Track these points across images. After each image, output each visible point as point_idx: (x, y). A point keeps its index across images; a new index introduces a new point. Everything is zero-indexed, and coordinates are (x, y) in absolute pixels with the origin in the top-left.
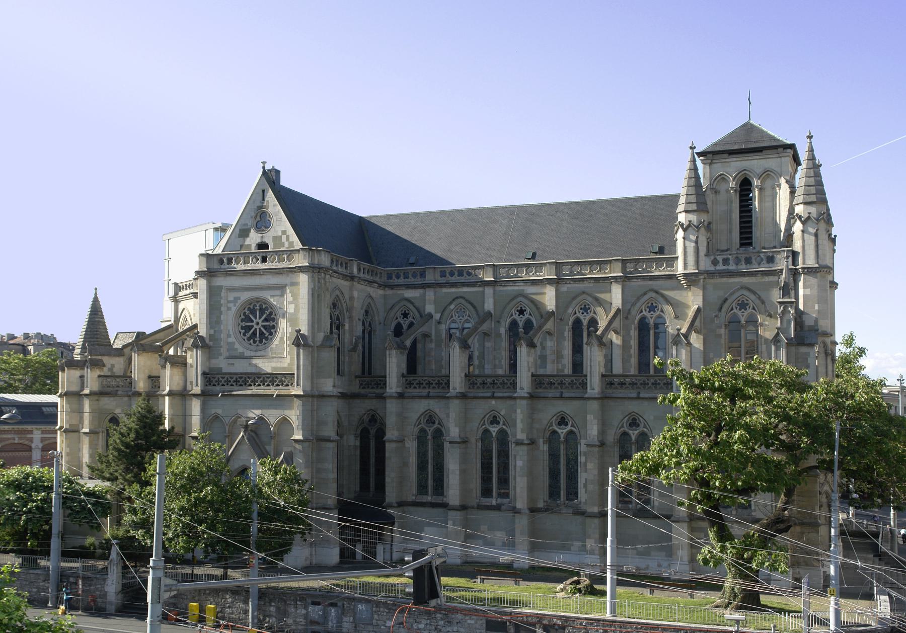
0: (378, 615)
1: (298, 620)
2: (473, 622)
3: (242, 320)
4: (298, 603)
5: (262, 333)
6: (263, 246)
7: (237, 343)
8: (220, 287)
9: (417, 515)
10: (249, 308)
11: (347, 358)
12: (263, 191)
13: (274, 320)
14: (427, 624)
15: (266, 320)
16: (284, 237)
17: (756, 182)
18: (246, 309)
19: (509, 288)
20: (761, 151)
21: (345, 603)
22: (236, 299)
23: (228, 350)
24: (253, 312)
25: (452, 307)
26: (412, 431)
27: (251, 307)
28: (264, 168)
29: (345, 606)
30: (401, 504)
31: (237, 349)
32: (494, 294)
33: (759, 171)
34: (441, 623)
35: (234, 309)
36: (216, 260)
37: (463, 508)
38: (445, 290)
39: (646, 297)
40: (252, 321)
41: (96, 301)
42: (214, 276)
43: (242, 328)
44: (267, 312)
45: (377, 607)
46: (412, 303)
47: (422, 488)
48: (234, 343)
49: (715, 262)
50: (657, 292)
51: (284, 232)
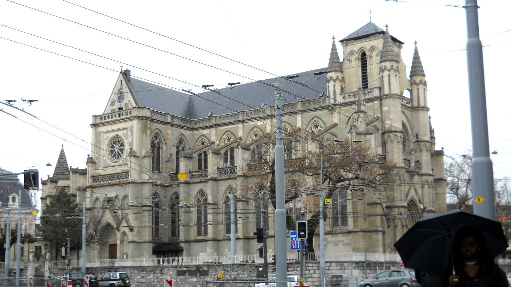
3: (111, 148)
6: (121, 109)
8: (101, 132)
9: (196, 246)
10: (113, 141)
11: (164, 166)
15: (120, 147)
16: (129, 103)
17: (368, 54)
19: (250, 123)
20: (368, 37)
22: (108, 137)
23: (104, 164)
24: (115, 143)
25: (224, 136)
26: (193, 201)
27: (114, 140)
28: (122, 69)
30: (187, 241)
32: (243, 127)
33: (369, 48)
34: (159, 274)
35: (107, 142)
36: (99, 118)
37: (214, 240)
38: (221, 128)
39: (313, 121)
41: (63, 151)
42: (98, 126)
45: (133, 269)
46: (206, 137)
47: (199, 233)
49: (344, 98)
50: (318, 117)
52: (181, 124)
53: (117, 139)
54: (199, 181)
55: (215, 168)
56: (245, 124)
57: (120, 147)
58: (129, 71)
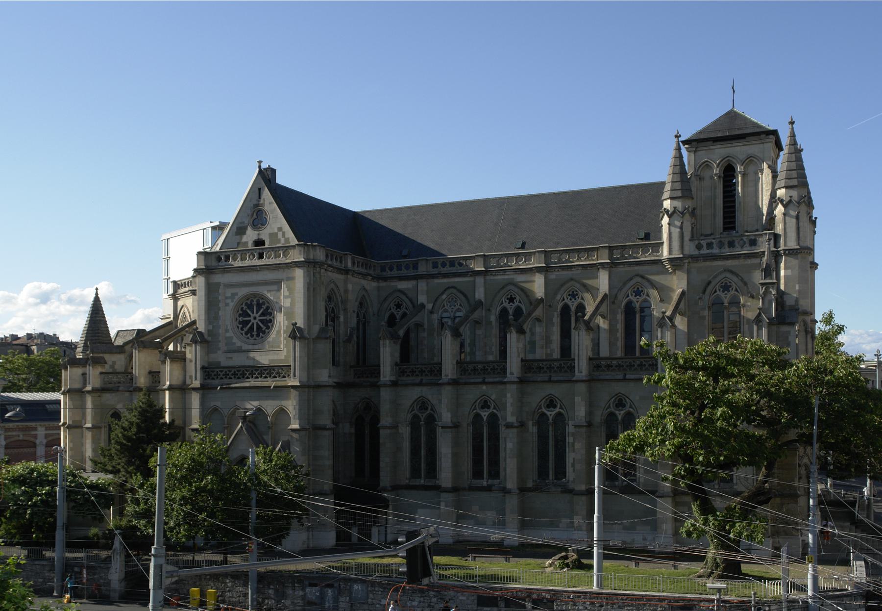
0: (373, 594)
1: (296, 601)
2: (464, 598)
4: (296, 585)
5: (259, 328)
6: (259, 243)
7: (234, 338)
8: (218, 284)
9: (410, 498)
12: (260, 189)
13: (270, 314)
14: (420, 602)
15: (263, 314)
18: (244, 304)
19: (499, 277)
21: (341, 583)
22: (234, 295)
24: (250, 307)
25: (444, 296)
28: (260, 167)
29: (342, 586)
31: (234, 344)
32: (485, 283)
33: (742, 157)
34: (434, 600)
35: (232, 304)
37: (455, 490)
38: (436, 281)
40: (250, 316)
41: (97, 300)
43: (240, 323)
44: (265, 307)
48: (231, 338)
51: (280, 229)
52: (363, 271)
53: (255, 300)
54: (418, 381)
55: (455, 362)
56: (488, 278)
57: (263, 314)
58: (273, 171)
